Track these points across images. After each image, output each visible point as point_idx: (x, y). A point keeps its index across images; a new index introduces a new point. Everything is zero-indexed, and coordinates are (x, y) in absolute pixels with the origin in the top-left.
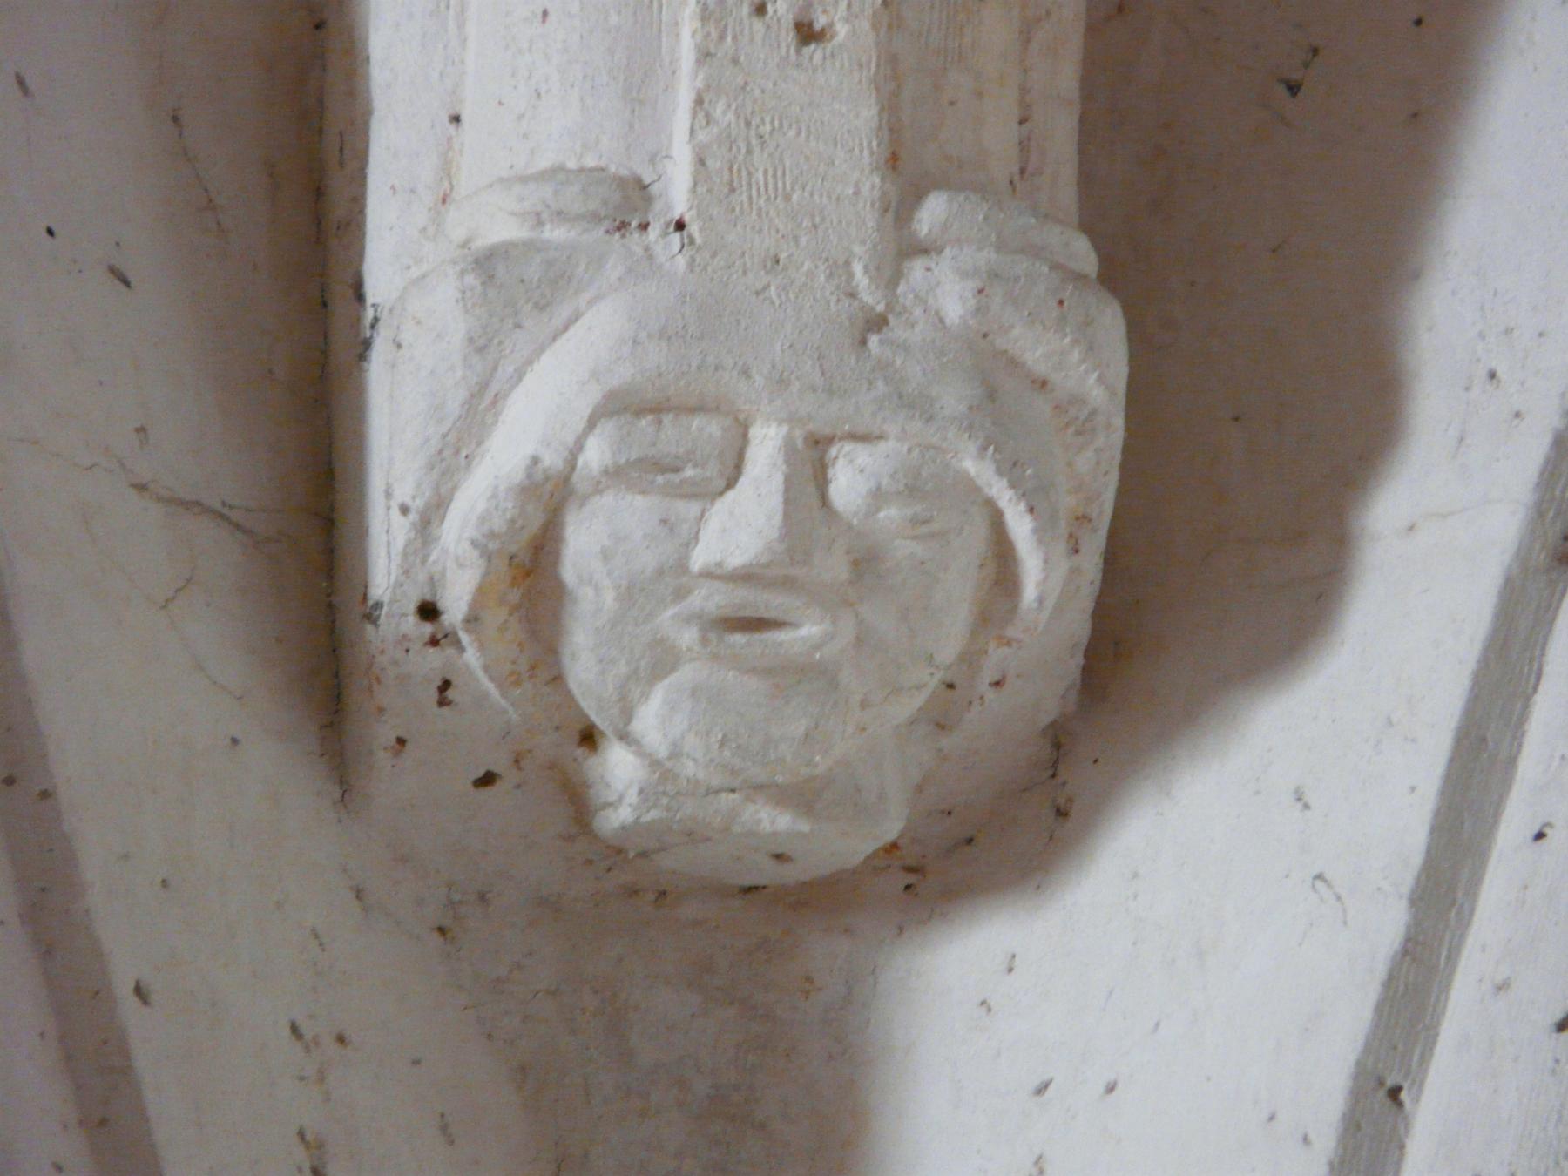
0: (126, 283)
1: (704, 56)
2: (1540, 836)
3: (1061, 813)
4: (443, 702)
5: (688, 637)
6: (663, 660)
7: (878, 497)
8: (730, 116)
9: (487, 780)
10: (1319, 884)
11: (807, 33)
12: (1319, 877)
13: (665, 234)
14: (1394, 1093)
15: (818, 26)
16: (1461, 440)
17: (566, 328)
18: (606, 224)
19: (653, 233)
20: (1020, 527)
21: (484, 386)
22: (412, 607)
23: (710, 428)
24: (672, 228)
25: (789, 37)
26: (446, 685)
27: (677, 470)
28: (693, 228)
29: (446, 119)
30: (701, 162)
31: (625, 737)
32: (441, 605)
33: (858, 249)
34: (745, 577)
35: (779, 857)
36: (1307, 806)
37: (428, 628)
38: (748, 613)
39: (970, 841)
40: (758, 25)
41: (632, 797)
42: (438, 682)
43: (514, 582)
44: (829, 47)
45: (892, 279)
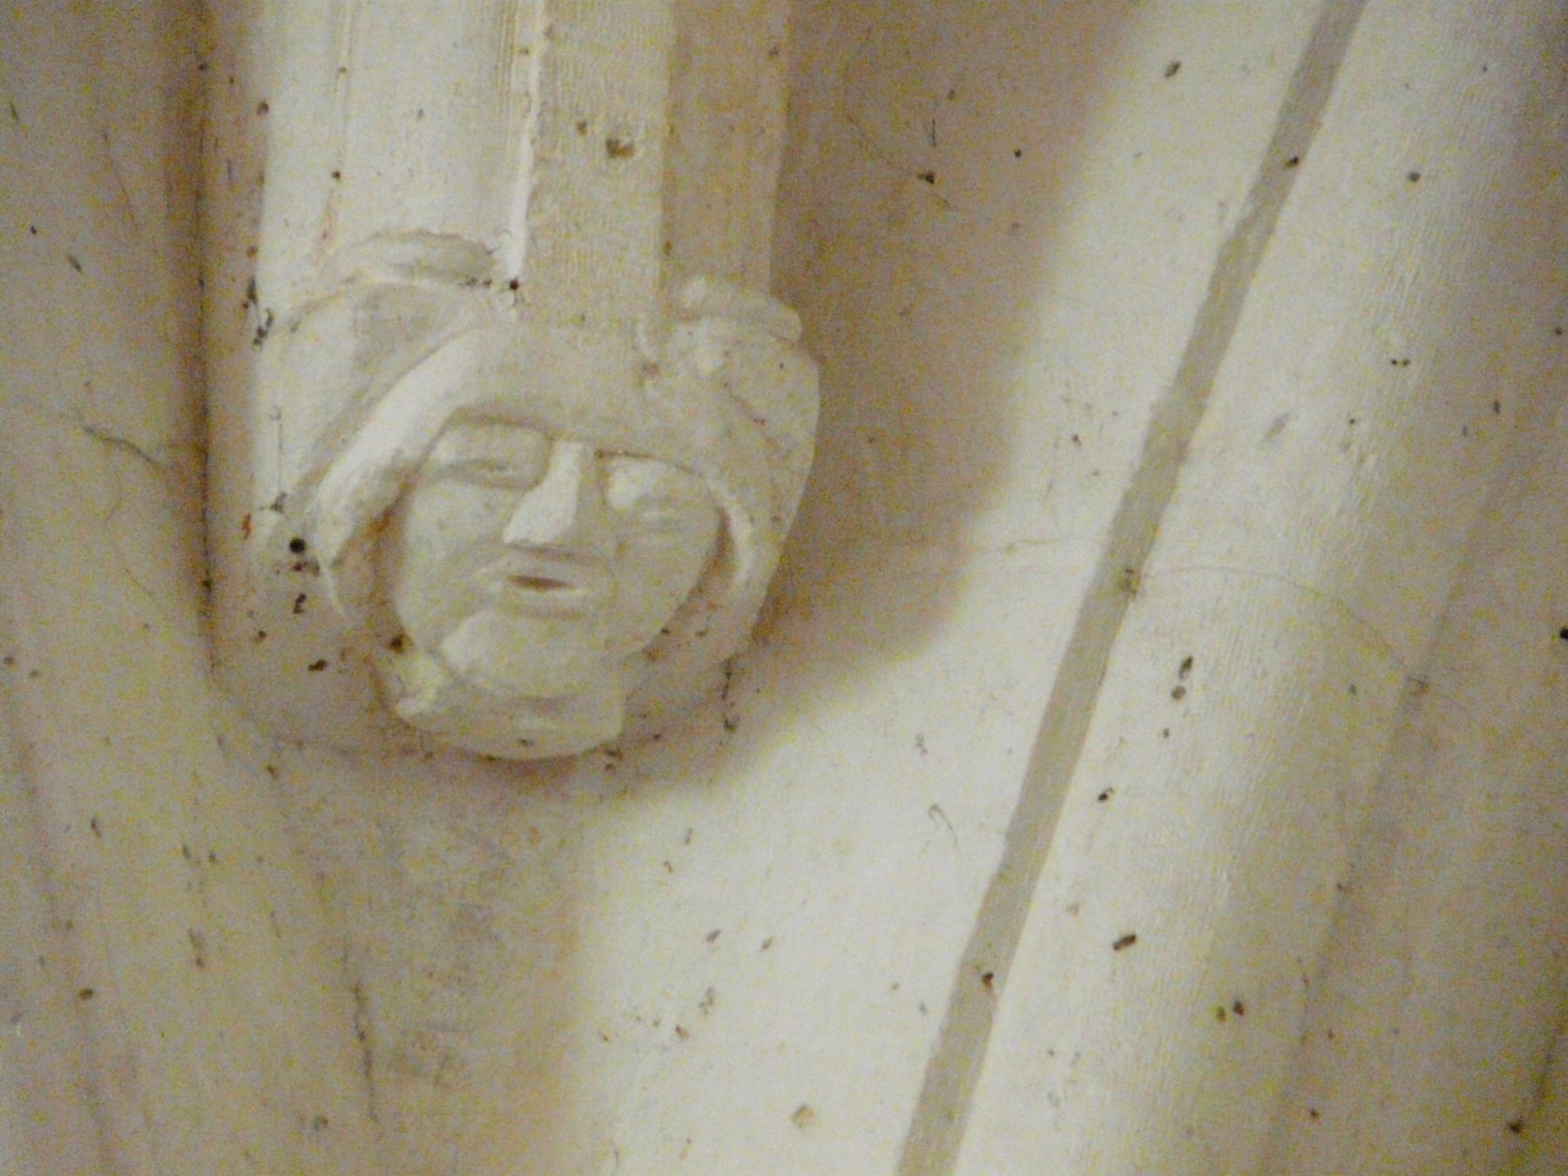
0: (78, 267)
1: (541, 161)
2: (1103, 797)
3: (729, 726)
4: (297, 610)
5: (496, 588)
6: (472, 601)
7: (644, 501)
8: (556, 207)
9: (319, 666)
10: (935, 813)
11: (615, 149)
12: (935, 808)
13: (502, 290)
14: (988, 978)
15: (622, 145)
16: (1050, 486)
17: (426, 357)
18: (462, 280)
19: (494, 289)
20: (741, 531)
21: (364, 390)
22: (286, 544)
23: (527, 440)
24: (507, 287)
25: (601, 150)
26: (302, 598)
27: (501, 468)
28: (524, 289)
29: (329, 176)
30: (532, 239)
31: (433, 652)
32: (308, 541)
33: (641, 316)
34: (542, 551)
35: (524, 742)
36: (925, 751)
37: (295, 558)
38: (540, 575)
39: (657, 737)
40: (580, 140)
41: (431, 695)
42: (297, 596)
43: (369, 536)
44: (630, 161)
45: (661, 335)
